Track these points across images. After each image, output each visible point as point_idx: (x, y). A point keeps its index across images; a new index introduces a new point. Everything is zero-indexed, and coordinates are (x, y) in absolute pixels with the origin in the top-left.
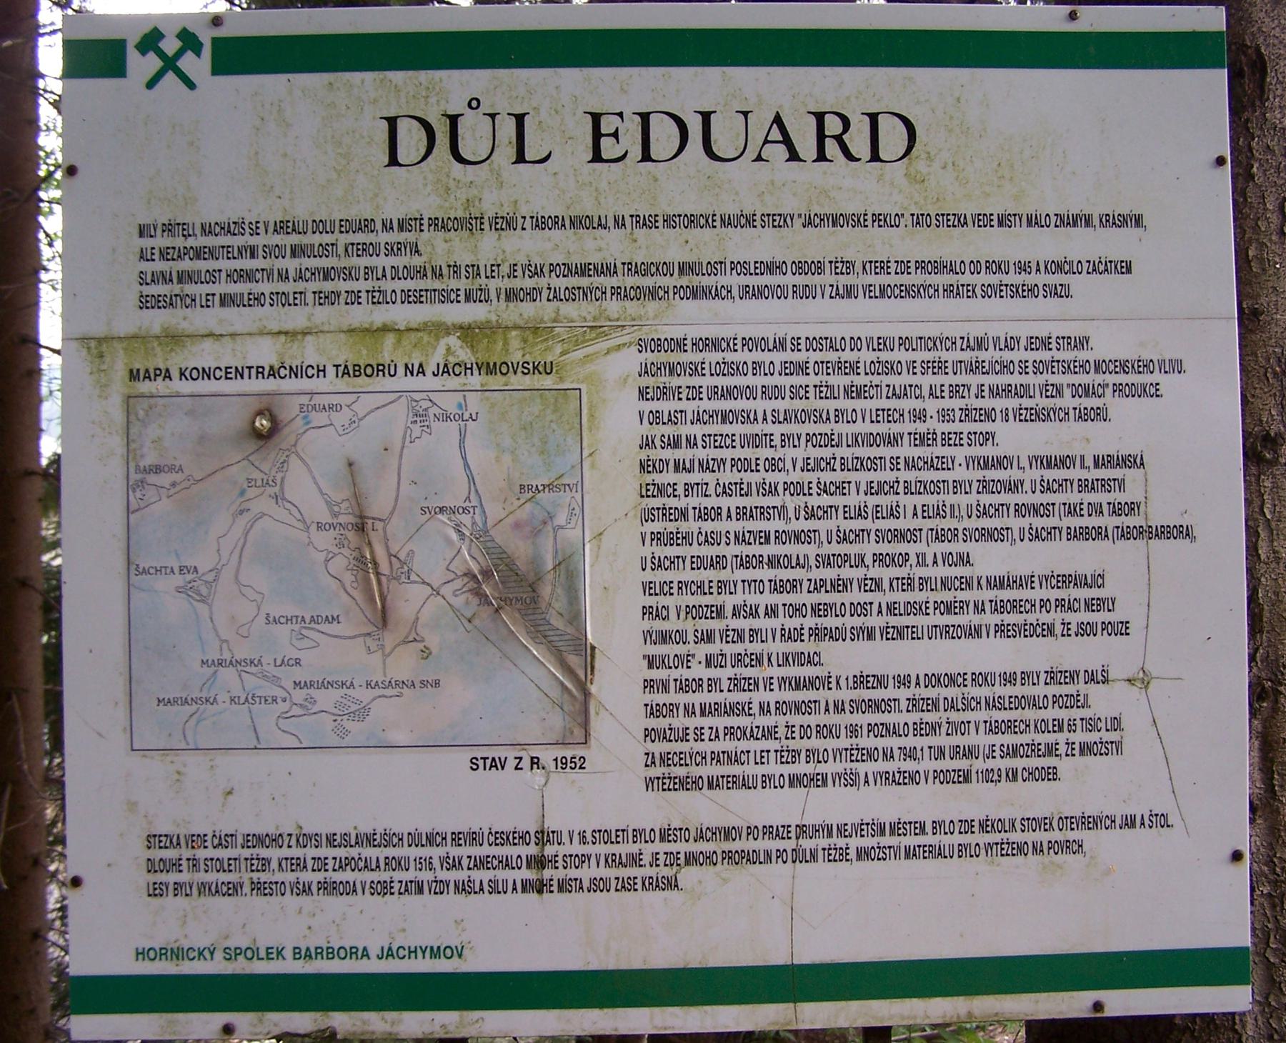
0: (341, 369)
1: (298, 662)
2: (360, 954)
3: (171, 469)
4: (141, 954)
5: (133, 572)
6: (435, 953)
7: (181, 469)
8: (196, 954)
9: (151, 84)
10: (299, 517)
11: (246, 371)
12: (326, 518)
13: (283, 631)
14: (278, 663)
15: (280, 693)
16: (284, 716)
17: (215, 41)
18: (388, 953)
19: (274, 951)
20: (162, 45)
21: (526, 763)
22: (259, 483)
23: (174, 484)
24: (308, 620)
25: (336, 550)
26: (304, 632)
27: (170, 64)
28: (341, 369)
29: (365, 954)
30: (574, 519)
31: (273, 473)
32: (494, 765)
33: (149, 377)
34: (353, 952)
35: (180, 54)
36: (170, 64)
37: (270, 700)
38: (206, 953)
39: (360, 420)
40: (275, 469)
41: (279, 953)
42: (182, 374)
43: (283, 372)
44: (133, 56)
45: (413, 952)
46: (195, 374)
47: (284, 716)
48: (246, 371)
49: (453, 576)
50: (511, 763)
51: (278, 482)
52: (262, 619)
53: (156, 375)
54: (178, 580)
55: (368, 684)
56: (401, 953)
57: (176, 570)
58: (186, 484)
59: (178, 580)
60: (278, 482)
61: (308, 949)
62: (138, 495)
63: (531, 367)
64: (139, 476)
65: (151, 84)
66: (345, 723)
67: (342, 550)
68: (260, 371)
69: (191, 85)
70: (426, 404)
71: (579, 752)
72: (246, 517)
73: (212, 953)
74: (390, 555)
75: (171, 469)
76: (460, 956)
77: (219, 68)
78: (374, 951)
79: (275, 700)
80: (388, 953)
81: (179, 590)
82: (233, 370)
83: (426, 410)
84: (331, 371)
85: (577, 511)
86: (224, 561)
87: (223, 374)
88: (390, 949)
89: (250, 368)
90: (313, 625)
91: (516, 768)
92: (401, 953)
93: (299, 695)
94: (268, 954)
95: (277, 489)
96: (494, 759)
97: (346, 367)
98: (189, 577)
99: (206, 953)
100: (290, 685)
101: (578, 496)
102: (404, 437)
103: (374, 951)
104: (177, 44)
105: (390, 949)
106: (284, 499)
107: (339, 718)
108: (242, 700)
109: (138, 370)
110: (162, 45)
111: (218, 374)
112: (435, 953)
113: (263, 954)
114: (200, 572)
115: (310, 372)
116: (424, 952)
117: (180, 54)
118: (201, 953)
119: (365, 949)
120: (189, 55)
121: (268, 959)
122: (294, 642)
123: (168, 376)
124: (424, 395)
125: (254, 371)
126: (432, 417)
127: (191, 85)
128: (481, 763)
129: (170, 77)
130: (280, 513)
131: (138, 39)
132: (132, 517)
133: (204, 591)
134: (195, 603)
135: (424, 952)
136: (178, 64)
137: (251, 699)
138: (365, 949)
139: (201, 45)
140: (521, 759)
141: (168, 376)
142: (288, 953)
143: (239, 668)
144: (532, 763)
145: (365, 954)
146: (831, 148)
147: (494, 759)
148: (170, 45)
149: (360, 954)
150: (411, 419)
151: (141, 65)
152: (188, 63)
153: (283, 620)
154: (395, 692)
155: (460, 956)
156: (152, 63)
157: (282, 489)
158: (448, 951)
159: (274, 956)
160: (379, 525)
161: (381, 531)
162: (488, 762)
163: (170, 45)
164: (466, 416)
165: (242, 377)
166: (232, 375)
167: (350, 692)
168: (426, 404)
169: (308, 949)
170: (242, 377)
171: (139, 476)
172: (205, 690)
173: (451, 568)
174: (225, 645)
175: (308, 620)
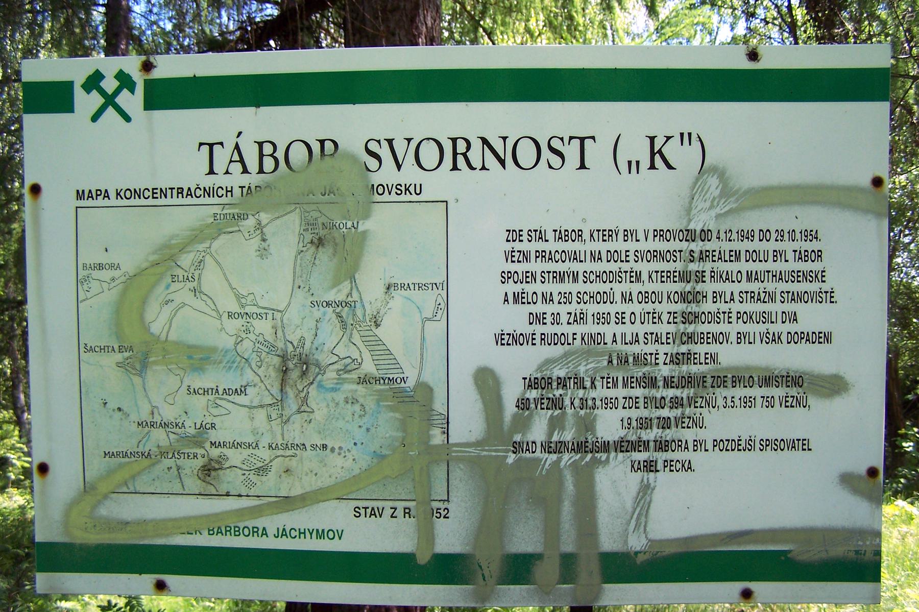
0: (245, 190)
2: (260, 532)
3: (112, 266)
5: (82, 350)
6: (321, 534)
7: (118, 267)
9: (95, 118)
10: (214, 307)
11: (169, 191)
12: (235, 308)
13: (202, 400)
17: (147, 82)
21: (400, 513)
22: (181, 278)
23: (113, 279)
24: (221, 392)
26: (218, 402)
27: (110, 100)
28: (245, 190)
29: (265, 533)
30: (440, 312)
31: (192, 271)
32: (373, 514)
33: (92, 197)
35: (117, 92)
36: (110, 100)
37: (192, 456)
40: (193, 267)
42: (118, 194)
44: (79, 93)
48: (169, 191)
51: (196, 278)
52: (184, 389)
53: (97, 195)
54: (119, 357)
55: (270, 446)
56: (293, 533)
59: (119, 357)
63: (403, 189)
64: (86, 273)
65: (95, 118)
66: (252, 477)
68: (180, 191)
69: (127, 119)
70: (315, 214)
72: (172, 306)
75: (112, 266)
76: (340, 538)
77: (150, 104)
81: (119, 365)
82: (158, 191)
85: (443, 306)
87: (150, 194)
88: (284, 530)
89: (172, 189)
90: (225, 396)
91: (392, 517)
92: (293, 533)
95: (195, 284)
96: (373, 509)
98: (127, 354)
101: (444, 293)
103: (271, 531)
104: (116, 84)
105: (284, 530)
106: (201, 292)
107: (247, 473)
109: (83, 191)
111: (147, 194)
112: (321, 534)
116: (311, 534)
117: (117, 92)
124: (314, 207)
125: (175, 192)
127: (127, 119)
128: (362, 511)
129: (110, 110)
130: (198, 303)
131: (83, 80)
135: (311, 534)
136: (116, 100)
138: (264, 529)
139: (134, 84)
140: (396, 509)
143: (168, 430)
144: (405, 513)
145: (265, 533)
147: (373, 509)
148: (110, 84)
149: (260, 532)
152: (124, 99)
155: (340, 538)
156: (96, 100)
157: (199, 283)
160: (280, 314)
162: (369, 511)
163: (110, 84)
165: (166, 197)
166: (158, 195)
167: (255, 452)
168: (315, 214)
170: (166, 197)
171: (86, 273)
172: (141, 446)
175: (221, 392)
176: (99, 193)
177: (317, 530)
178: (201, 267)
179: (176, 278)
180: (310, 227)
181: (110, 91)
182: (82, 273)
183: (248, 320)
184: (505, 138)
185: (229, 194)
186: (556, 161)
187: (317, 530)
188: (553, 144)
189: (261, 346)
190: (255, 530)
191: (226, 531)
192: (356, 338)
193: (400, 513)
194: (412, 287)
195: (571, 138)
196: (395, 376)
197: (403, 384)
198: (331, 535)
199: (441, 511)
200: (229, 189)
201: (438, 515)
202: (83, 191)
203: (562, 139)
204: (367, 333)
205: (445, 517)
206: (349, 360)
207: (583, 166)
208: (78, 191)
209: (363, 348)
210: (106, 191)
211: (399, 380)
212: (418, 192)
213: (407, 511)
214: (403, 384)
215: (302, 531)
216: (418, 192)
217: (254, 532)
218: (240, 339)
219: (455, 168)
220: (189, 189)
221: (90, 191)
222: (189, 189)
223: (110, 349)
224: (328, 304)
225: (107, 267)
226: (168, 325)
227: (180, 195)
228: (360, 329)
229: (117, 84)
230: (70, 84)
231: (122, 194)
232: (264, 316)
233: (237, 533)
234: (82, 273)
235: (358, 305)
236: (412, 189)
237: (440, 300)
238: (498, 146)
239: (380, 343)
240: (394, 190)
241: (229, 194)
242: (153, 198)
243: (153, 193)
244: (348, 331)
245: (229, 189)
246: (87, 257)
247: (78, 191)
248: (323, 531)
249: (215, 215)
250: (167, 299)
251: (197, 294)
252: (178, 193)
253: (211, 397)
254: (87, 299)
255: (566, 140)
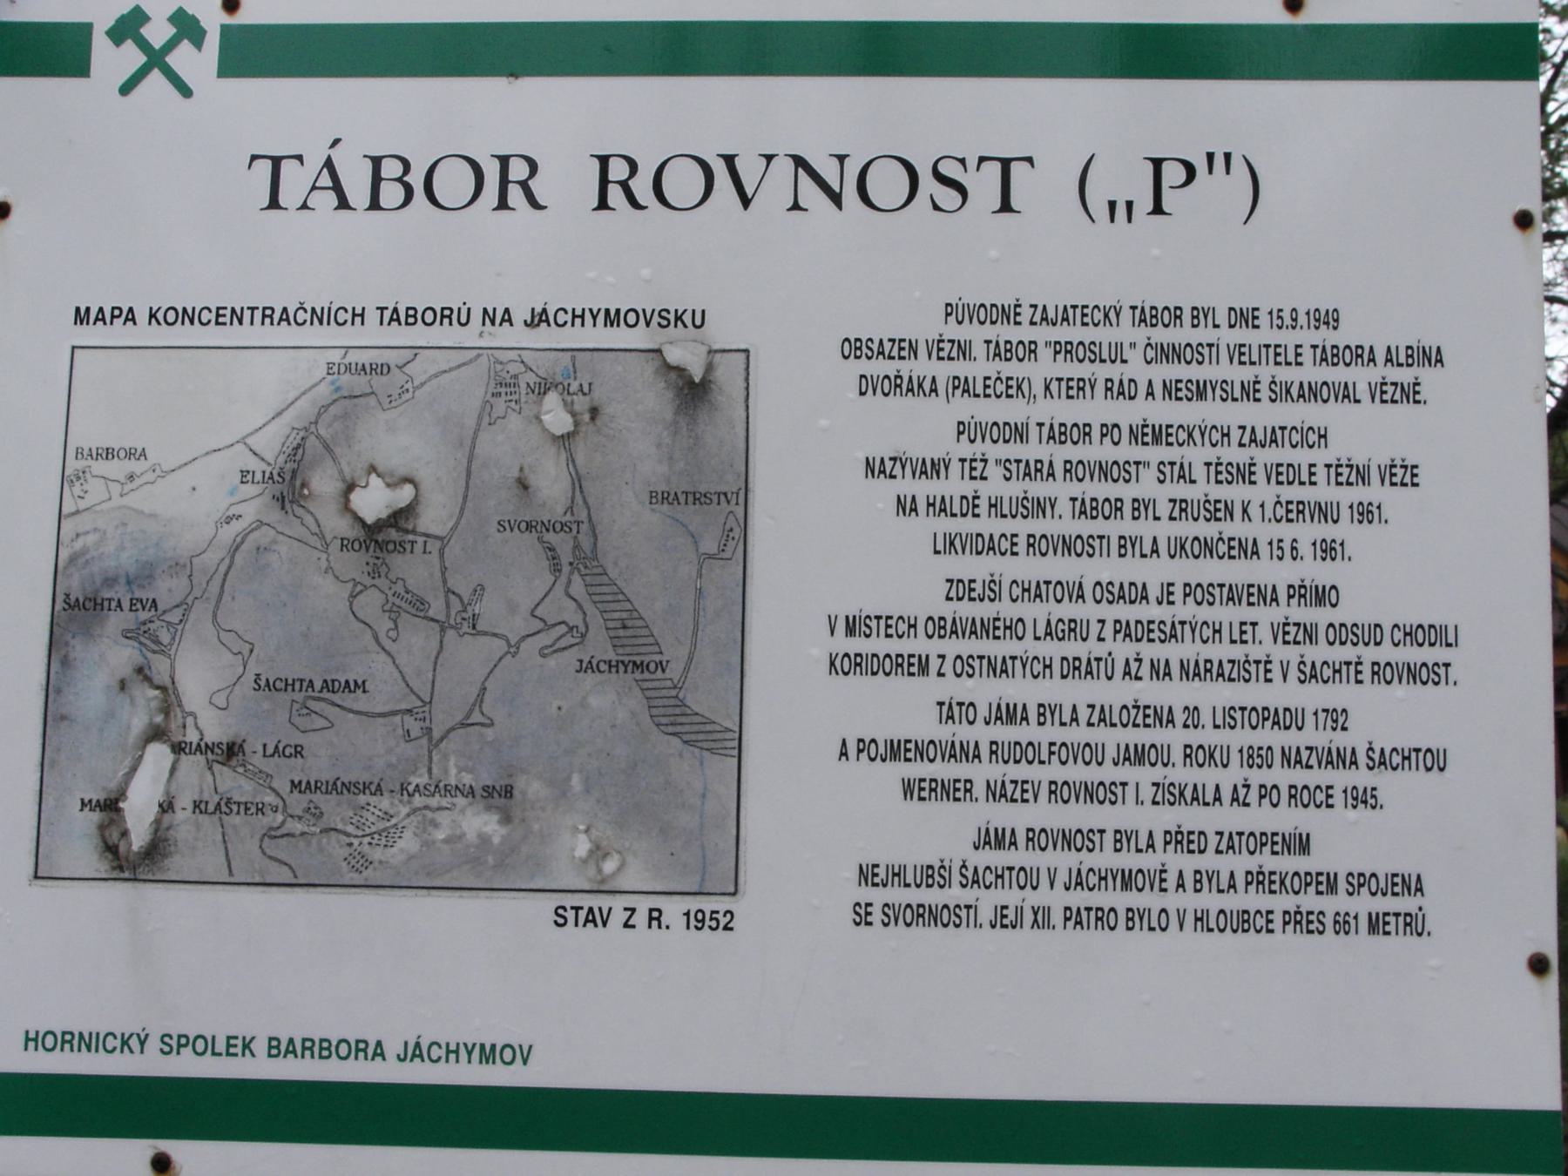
1: (298, 751)
2: (370, 1052)
4: (32, 1040)
6: (488, 1054)
8: (118, 1043)
9: (126, 89)
10: (314, 528)
11: (247, 314)
14: (270, 750)
15: (270, 798)
16: (271, 834)
17: (226, 30)
18: (415, 1052)
19: (239, 1042)
20: (145, 31)
21: (640, 918)
22: (259, 477)
23: (131, 477)
25: (368, 581)
28: (387, 314)
29: (379, 1051)
30: (731, 544)
32: (590, 920)
33: (103, 320)
34: (360, 1048)
35: (171, 45)
36: (156, 59)
38: (134, 1042)
39: (416, 388)
41: (246, 1046)
42: (152, 316)
43: (301, 316)
44: (101, 45)
45: (452, 1052)
46: (171, 316)
47: (271, 834)
48: (247, 314)
49: (540, 625)
50: (618, 917)
53: (113, 317)
57: (126, 604)
58: (150, 477)
60: (288, 477)
61: (291, 1041)
62: (77, 490)
63: (672, 317)
64: (81, 464)
65: (126, 89)
67: (376, 582)
68: (267, 314)
69: (186, 92)
70: (519, 368)
71: (721, 904)
73: (142, 1043)
74: (449, 591)
76: (525, 1062)
78: (393, 1048)
79: (260, 810)
80: (415, 1052)
82: (228, 312)
83: (516, 376)
84: (372, 316)
85: (737, 533)
86: (197, 592)
87: (213, 316)
88: (418, 1045)
89: (253, 309)
90: (325, 695)
91: (626, 925)
92: (435, 1053)
93: (298, 802)
94: (229, 1046)
96: (591, 910)
97: (395, 310)
98: (144, 615)
99: (134, 1042)
100: (284, 788)
101: (740, 511)
102: (480, 418)
103: (393, 1048)
104: (171, 31)
105: (418, 1045)
107: (356, 842)
108: (211, 808)
109: (88, 309)
110: (145, 31)
112: (488, 1054)
113: (221, 1046)
114: (161, 607)
115: (342, 316)
116: (470, 1053)
117: (171, 45)
118: (125, 1043)
119: (379, 1044)
120: (186, 46)
121: (228, 1054)
122: (296, 720)
123: (131, 317)
124: (513, 355)
125: (258, 315)
126: (523, 386)
127: (186, 92)
128: (570, 915)
129: (156, 76)
132: (66, 525)
133: (165, 637)
134: (149, 655)
135: (470, 1053)
136: (144, 59)
137: (225, 806)
138: (379, 1044)
139: (203, 33)
140: (633, 910)
141: (131, 317)
142: (260, 1047)
144: (651, 919)
146: (515, 195)
147: (591, 910)
150: (491, 390)
151: (112, 61)
152: (182, 58)
153: (279, 685)
154: (445, 802)
155: (525, 1062)
156: (132, 57)
158: (508, 1052)
159: (239, 1050)
161: (436, 554)
162: (582, 914)
163: (158, 32)
164: (574, 387)
165: (241, 323)
166: (227, 320)
168: (519, 368)
169: (291, 1041)
170: (241, 323)
171: (81, 464)
173: (537, 613)
174: (190, 720)
176: (117, 312)
177: (607, 311)
178: (298, 457)
179: (249, 477)
180: (503, 390)
181: (157, 44)
182: (73, 466)
183: (379, 553)
184: (841, 159)
185: (358, 320)
186: (949, 198)
187: (607, 311)
188: (944, 168)
189: (398, 602)
190: (362, 1046)
191: (304, 1048)
192: (578, 588)
193: (640, 918)
194: (682, 498)
195: (982, 159)
196: (646, 659)
197: (659, 674)
198: (508, 1055)
199: (719, 916)
200: (358, 311)
201: (714, 924)
202: (88, 309)
203: (962, 161)
204: (598, 580)
205: (726, 928)
206: (563, 628)
207: (1006, 207)
208: (78, 309)
209: (588, 606)
210: (131, 310)
211: (652, 667)
212: (698, 322)
213: (655, 914)
214: (659, 674)
215: (578, 312)
216: (698, 322)
217: (358, 1050)
218: (359, 588)
219: (503, 204)
220: (285, 310)
221: (101, 310)
222: (285, 310)
223: (114, 604)
224: (529, 526)
225: (122, 454)
226: (227, 561)
227: (268, 320)
228: (583, 571)
229: (172, 31)
230: (85, 30)
231: (160, 316)
232: (408, 547)
233: (325, 1053)
234: (73, 466)
235: (584, 527)
236: (687, 318)
237: (731, 523)
238: (830, 173)
239: (621, 597)
240: (656, 319)
241: (358, 320)
242: (217, 323)
243: (218, 316)
244: (563, 579)
245: (358, 311)
246: (87, 435)
247: (78, 309)
248: (493, 1047)
249: (330, 365)
250: (230, 513)
251: (288, 505)
252: (264, 316)
253: (299, 696)
254: (78, 512)
255: (972, 163)
